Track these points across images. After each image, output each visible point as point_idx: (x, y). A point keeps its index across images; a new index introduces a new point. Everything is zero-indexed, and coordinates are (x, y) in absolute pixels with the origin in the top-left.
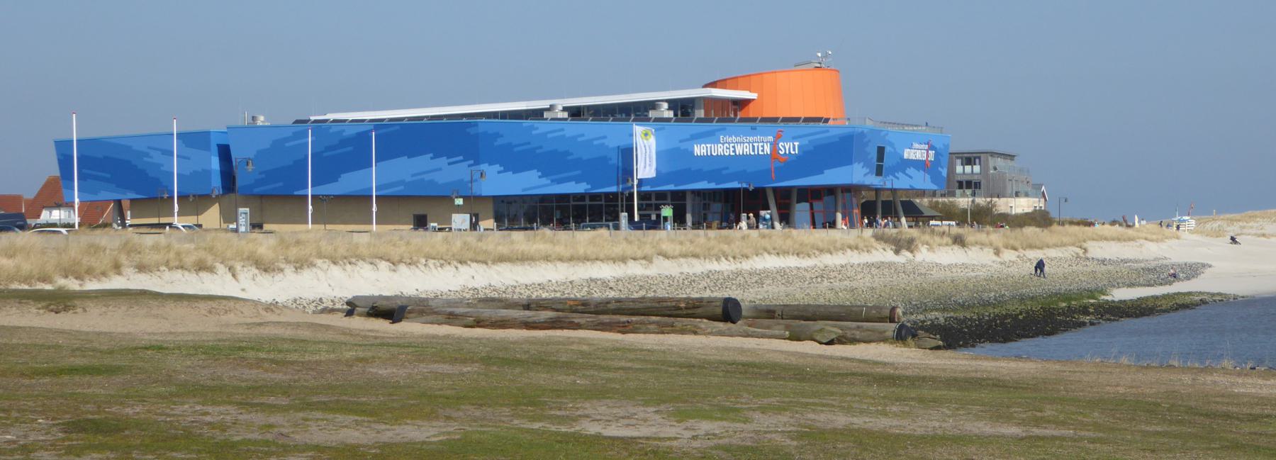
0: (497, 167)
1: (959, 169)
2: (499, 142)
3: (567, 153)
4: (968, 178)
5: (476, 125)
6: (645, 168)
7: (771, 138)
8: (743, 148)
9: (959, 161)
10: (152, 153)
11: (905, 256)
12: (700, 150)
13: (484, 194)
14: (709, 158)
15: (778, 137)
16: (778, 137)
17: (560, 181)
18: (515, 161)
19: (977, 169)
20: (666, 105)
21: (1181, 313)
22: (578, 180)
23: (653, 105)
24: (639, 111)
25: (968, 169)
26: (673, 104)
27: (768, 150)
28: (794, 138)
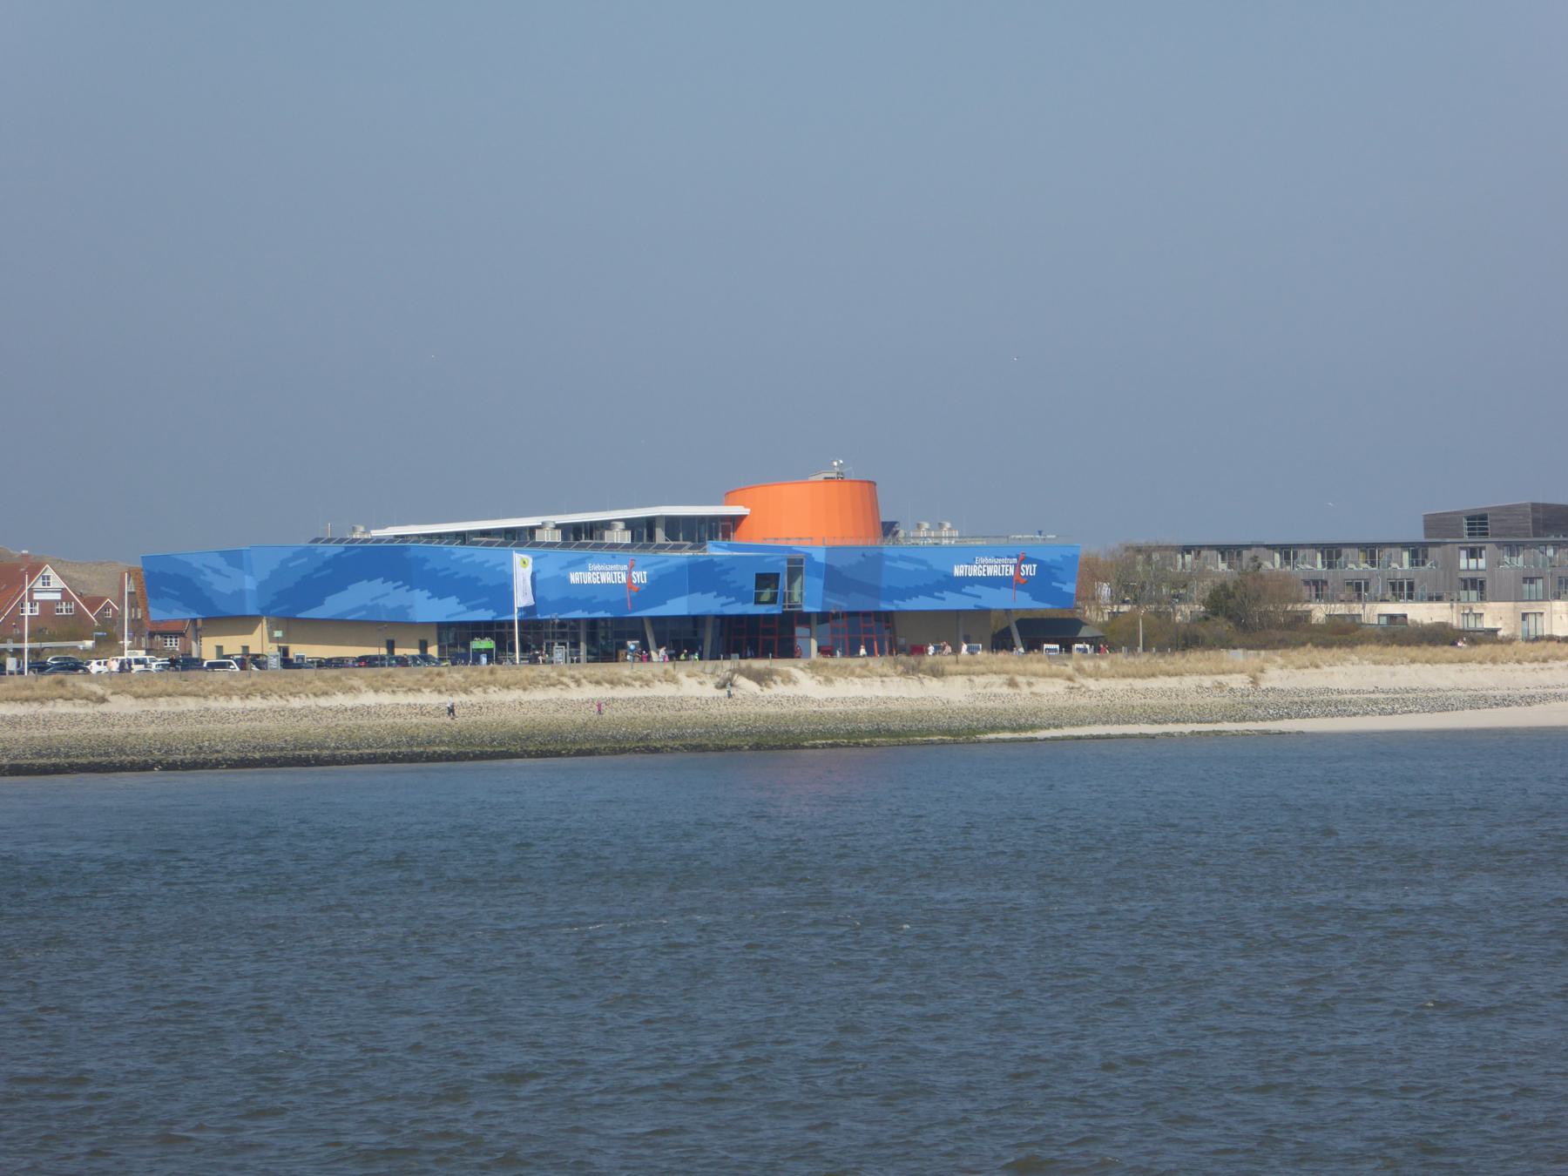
0: (426, 593)
1: (1463, 563)
2: (427, 567)
3: (477, 579)
4: (1473, 575)
5: (407, 549)
6: (522, 597)
7: (625, 567)
8: (606, 578)
9: (1463, 553)
10: (208, 571)
11: (103, 708)
12: (575, 578)
13: (419, 620)
14: (581, 586)
15: (631, 567)
16: (631, 567)
17: (473, 608)
18: (440, 586)
19: (1482, 563)
20: (621, 525)
21: (834, 750)
22: (486, 607)
23: (607, 525)
24: (514, 537)
25: (1473, 562)
26: (630, 524)
27: (624, 579)
28: (644, 567)
